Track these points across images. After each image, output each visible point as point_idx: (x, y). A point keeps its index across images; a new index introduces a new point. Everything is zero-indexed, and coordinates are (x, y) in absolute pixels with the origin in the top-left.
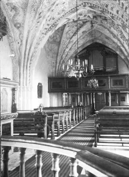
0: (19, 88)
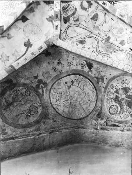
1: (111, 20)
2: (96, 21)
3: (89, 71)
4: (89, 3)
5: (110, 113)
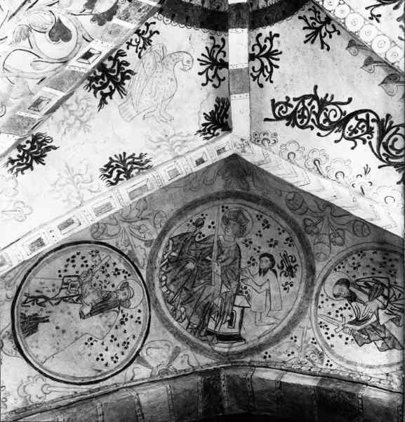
1: (42, 76)
2: (47, 34)
4: (105, 15)
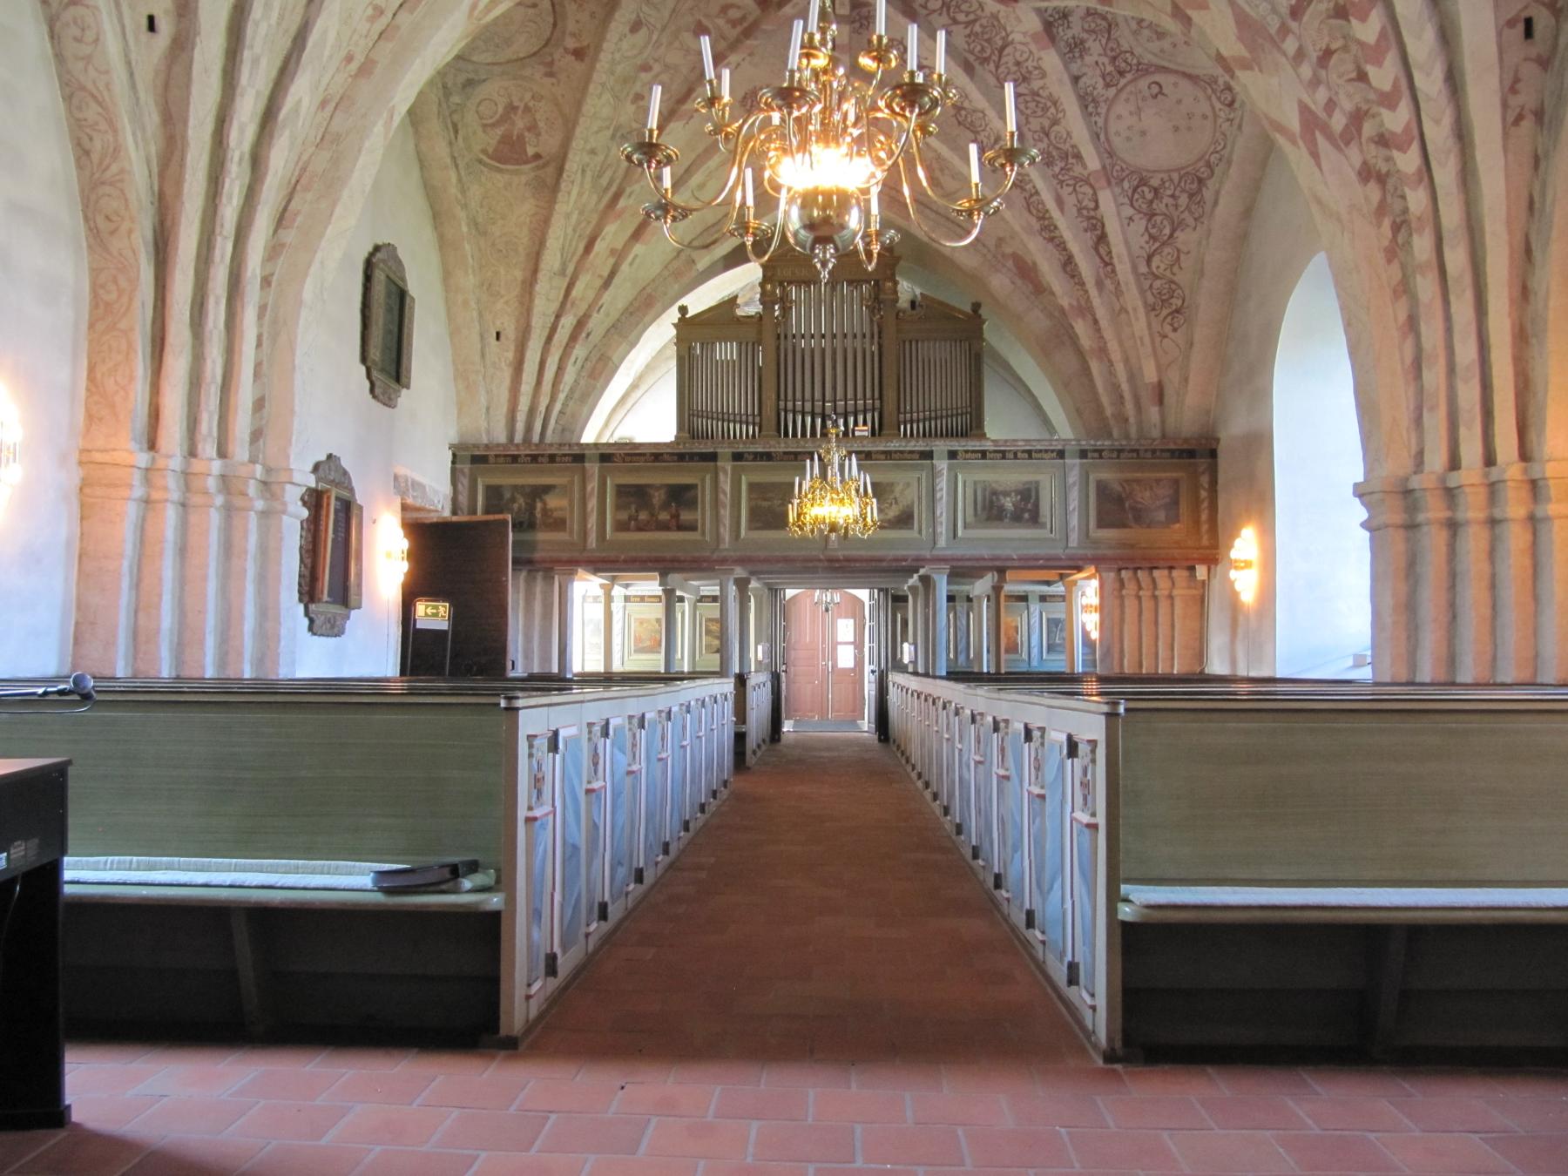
0: (265, 514)
3: (566, 49)
5: (479, 104)
